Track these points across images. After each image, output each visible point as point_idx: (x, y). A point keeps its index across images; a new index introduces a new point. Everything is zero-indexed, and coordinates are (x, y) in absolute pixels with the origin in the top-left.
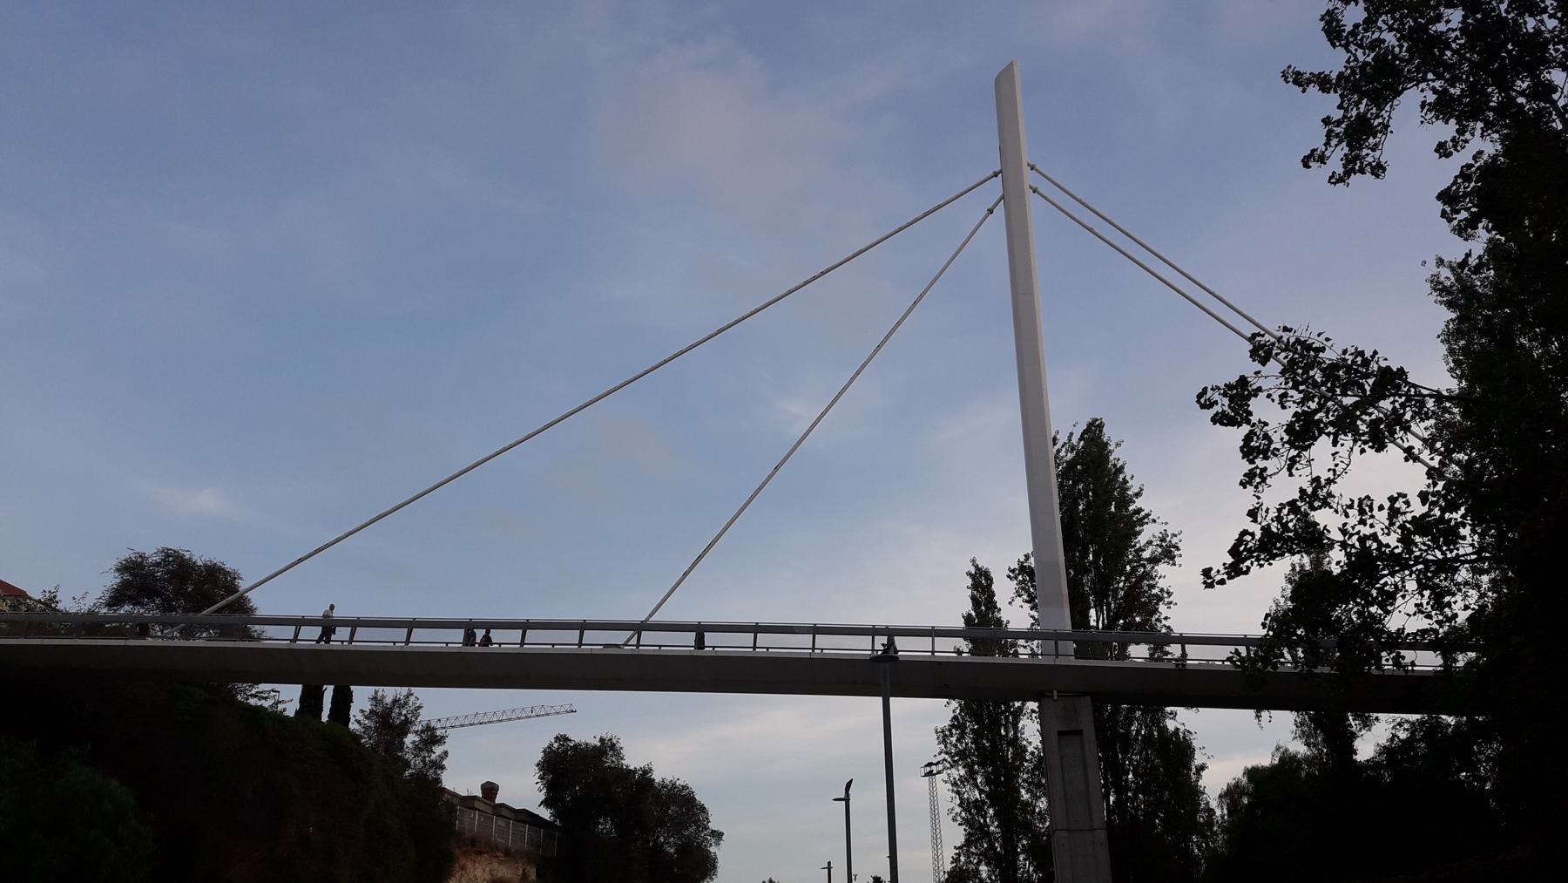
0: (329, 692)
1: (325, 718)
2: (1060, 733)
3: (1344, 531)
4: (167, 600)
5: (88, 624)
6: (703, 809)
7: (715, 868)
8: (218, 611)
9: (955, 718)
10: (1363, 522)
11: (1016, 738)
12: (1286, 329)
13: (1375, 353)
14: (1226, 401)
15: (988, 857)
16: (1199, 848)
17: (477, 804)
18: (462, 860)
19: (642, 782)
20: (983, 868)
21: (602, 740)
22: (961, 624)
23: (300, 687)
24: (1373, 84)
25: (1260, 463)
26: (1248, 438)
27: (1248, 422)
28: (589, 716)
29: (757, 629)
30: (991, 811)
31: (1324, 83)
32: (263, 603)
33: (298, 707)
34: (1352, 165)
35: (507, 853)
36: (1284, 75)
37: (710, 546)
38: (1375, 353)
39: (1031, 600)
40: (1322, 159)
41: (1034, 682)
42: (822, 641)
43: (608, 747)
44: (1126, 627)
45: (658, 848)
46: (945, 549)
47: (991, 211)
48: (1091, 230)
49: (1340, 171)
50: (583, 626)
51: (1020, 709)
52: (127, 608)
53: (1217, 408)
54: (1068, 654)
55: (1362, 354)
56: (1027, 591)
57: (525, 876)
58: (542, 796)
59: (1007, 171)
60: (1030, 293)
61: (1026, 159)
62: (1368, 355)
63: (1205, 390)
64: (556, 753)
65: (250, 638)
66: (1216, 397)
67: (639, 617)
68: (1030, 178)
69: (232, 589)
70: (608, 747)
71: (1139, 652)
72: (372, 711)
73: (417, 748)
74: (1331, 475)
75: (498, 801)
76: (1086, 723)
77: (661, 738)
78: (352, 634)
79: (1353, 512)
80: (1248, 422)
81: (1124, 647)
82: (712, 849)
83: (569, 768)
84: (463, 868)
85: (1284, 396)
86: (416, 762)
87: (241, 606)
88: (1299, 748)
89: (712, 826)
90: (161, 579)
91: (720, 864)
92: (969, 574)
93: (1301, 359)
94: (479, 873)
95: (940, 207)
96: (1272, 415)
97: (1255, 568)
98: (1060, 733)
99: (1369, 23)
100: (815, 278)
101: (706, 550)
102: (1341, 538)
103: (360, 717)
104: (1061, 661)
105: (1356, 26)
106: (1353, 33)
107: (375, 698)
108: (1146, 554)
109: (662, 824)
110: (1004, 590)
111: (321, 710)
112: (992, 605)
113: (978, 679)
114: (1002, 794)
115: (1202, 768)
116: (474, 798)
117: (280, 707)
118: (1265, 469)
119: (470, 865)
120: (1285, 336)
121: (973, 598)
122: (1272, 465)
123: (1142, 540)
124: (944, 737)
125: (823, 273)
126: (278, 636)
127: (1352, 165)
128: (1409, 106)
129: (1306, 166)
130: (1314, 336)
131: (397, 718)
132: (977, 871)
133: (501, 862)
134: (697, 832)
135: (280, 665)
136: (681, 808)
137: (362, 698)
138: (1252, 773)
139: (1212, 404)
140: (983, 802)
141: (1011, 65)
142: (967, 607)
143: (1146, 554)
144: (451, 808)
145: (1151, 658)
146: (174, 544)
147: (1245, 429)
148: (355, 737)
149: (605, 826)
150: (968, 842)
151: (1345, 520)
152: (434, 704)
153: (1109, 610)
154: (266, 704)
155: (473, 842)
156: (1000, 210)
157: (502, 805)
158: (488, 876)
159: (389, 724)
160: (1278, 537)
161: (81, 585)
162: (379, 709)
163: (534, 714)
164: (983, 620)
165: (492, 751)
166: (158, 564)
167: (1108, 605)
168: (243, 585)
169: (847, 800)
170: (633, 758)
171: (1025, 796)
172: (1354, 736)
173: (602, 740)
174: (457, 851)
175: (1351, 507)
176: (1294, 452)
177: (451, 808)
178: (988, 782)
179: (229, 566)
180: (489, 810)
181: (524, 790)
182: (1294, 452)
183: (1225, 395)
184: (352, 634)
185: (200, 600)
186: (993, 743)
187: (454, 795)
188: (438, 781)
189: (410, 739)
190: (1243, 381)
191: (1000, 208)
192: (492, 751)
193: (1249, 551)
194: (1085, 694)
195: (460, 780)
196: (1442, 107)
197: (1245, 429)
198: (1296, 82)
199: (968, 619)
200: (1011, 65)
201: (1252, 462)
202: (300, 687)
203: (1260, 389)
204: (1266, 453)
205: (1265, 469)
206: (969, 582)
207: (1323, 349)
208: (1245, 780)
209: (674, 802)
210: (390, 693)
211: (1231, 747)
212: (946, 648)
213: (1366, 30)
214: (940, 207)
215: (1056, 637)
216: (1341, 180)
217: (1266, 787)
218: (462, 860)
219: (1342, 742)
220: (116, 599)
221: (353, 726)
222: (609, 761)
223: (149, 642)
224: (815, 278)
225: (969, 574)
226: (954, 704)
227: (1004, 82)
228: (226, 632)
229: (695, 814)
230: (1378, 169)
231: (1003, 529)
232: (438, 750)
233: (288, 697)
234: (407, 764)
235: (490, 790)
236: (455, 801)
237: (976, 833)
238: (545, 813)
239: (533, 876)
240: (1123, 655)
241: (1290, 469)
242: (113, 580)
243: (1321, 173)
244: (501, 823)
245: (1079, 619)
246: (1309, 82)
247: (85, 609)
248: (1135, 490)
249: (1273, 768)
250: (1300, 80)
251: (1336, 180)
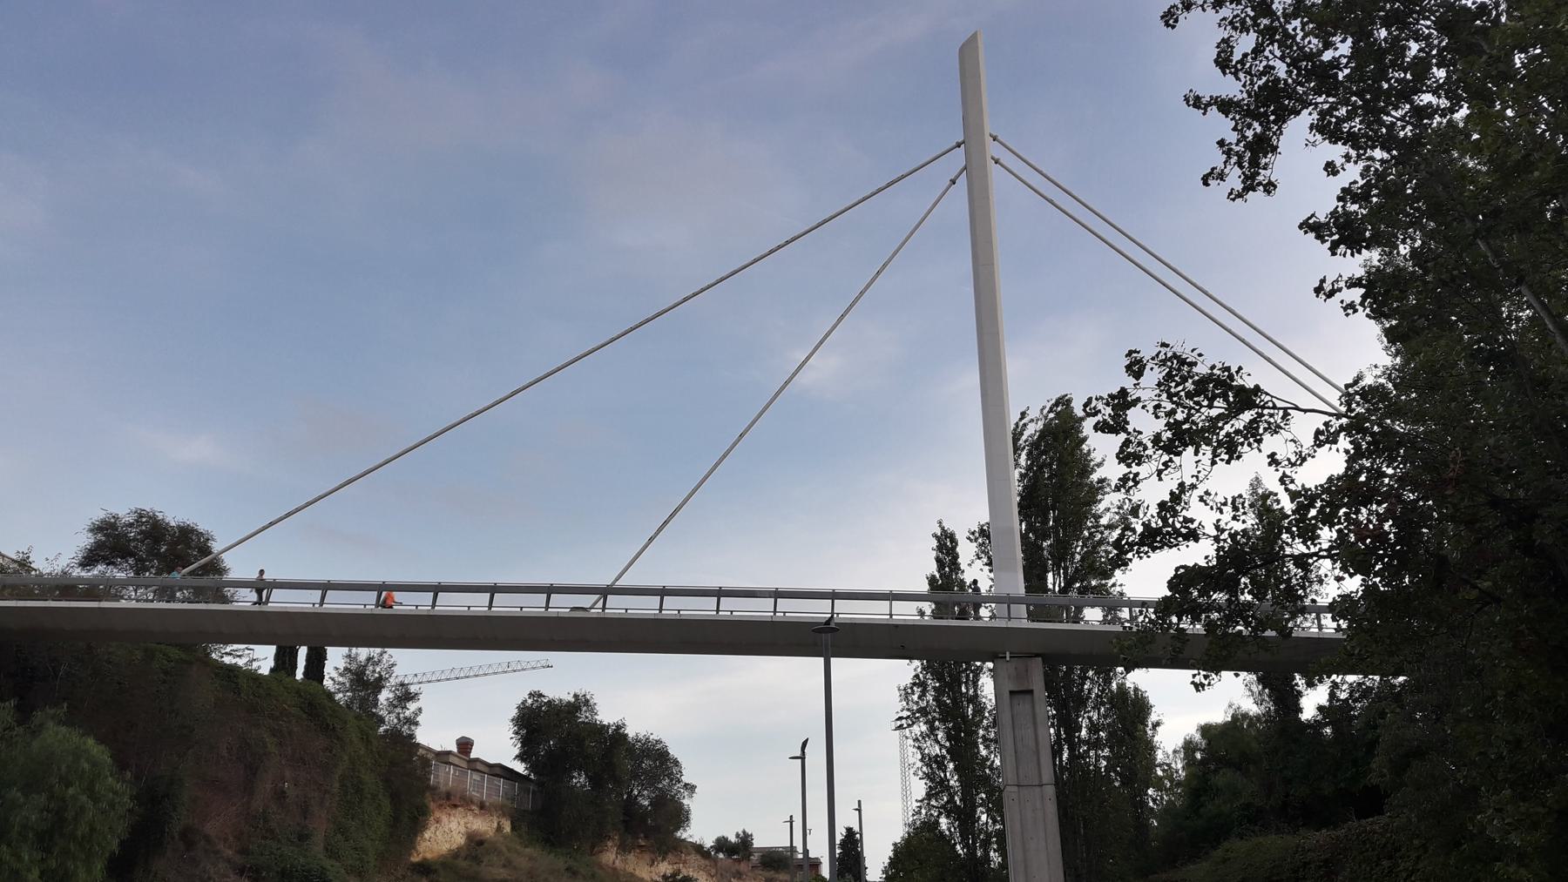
0: (303, 652)
1: (299, 675)
2: (1012, 693)
3: (1217, 527)
4: (140, 560)
5: (64, 587)
6: (676, 763)
7: (688, 819)
8: (191, 573)
9: (917, 676)
10: (1234, 518)
11: (976, 696)
12: (1164, 345)
13: (1240, 368)
14: (1109, 410)
15: (949, 810)
16: (1154, 800)
17: (452, 759)
18: (437, 814)
19: (616, 737)
20: (943, 821)
21: (576, 696)
22: (924, 587)
23: (274, 648)
24: (1266, 108)
25: (1135, 469)
26: (1127, 443)
27: (1125, 430)
28: (561, 675)
29: (720, 593)
30: (951, 766)
31: (1225, 106)
32: (239, 566)
33: (272, 664)
34: (1250, 184)
35: (482, 806)
36: (1187, 100)
37: (676, 512)
38: (1240, 368)
39: (989, 564)
40: (1221, 176)
41: (993, 645)
42: (783, 604)
43: (581, 703)
44: (1082, 591)
45: (632, 800)
46: (912, 515)
47: (953, 182)
48: (1051, 202)
49: (1239, 187)
50: (550, 590)
51: (981, 668)
52: (101, 567)
53: (1099, 417)
54: (1020, 619)
55: (1228, 369)
56: (987, 553)
57: (499, 828)
58: (517, 751)
59: (971, 141)
60: (990, 264)
61: (988, 129)
62: (1233, 370)
63: (1090, 400)
64: (530, 708)
65: (225, 600)
66: (1100, 406)
67: (605, 580)
68: (993, 149)
69: (205, 551)
70: (581, 703)
71: (1093, 615)
72: (346, 669)
73: (392, 706)
74: (1194, 480)
75: (473, 756)
76: (1038, 684)
77: (632, 696)
78: (323, 598)
79: (1228, 509)
80: (1125, 430)
81: (1079, 610)
82: (685, 802)
83: (546, 726)
84: (438, 821)
85: (1157, 407)
86: (391, 719)
87: (215, 568)
88: (1251, 707)
89: (685, 779)
90: (135, 539)
91: (692, 816)
92: (935, 535)
93: (1177, 367)
94: (454, 826)
95: (903, 177)
96: (1145, 423)
97: (1136, 560)
98: (1012, 693)
99: (1258, 51)
100: (780, 247)
101: (672, 516)
102: (1215, 533)
103: (334, 674)
104: (1013, 624)
105: (1245, 55)
106: (1242, 62)
107: (349, 656)
108: (1104, 521)
109: (636, 777)
110: (966, 551)
111: (295, 667)
112: (955, 566)
113: (942, 644)
114: (962, 748)
115: (1156, 725)
116: (449, 753)
117: (255, 665)
118: (1137, 474)
119: (445, 819)
120: (1164, 350)
121: (938, 560)
122: (1144, 470)
123: (1101, 507)
124: (906, 694)
125: (788, 242)
126: (245, 600)
127: (1250, 184)
128: (1299, 127)
129: (1206, 184)
130: (1188, 351)
131: (371, 674)
132: (937, 823)
133: (475, 815)
134: (671, 785)
135: (252, 628)
136: (655, 761)
137: (336, 658)
138: (1206, 730)
139: (1097, 412)
140: (944, 757)
141: (974, 37)
142: (932, 568)
143: (1104, 521)
144: (425, 762)
145: (1104, 622)
146: (147, 506)
147: (1123, 436)
148: (330, 695)
149: (580, 780)
150: (929, 796)
151: (1218, 515)
152: (406, 663)
153: (1065, 574)
154: (241, 662)
155: (448, 796)
156: (962, 181)
157: (477, 760)
158: (463, 829)
159: (364, 683)
160: (1158, 531)
161: (56, 549)
162: (354, 667)
163: (509, 669)
164: (946, 582)
165: (466, 709)
166: (131, 525)
167: (1066, 569)
168: (216, 547)
169: (803, 758)
170: (606, 715)
171: (984, 752)
172: (1300, 694)
173: (576, 696)
174: (432, 805)
175: (1225, 504)
176: (1166, 458)
177: (425, 762)
178: (949, 738)
179: (201, 528)
180: (464, 765)
181: (500, 746)
182: (1166, 458)
183: (1108, 404)
184: (323, 598)
185: (174, 561)
186: (954, 700)
187: (429, 750)
188: (412, 736)
189: (385, 696)
190: (1123, 392)
191: (963, 179)
192: (466, 709)
193: (1131, 545)
194: (1037, 655)
195: (434, 734)
196: (1328, 129)
197: (1123, 436)
198: (1195, 106)
199: (932, 580)
200: (974, 37)
201: (1129, 466)
202: (274, 648)
203: (1138, 400)
204: (1138, 459)
205: (1137, 474)
206: (935, 543)
207: (1195, 364)
208: (1197, 737)
209: (648, 757)
210: (363, 653)
211: (1185, 708)
212: (906, 612)
213: (1254, 59)
214: (903, 177)
215: (1009, 600)
216: (1240, 195)
217: (1220, 745)
218: (437, 814)
219: (1287, 701)
220: (89, 560)
221: (327, 683)
222: (583, 716)
223: (123, 604)
224: (780, 247)
225: (935, 535)
226: (917, 663)
227: (968, 52)
228: (199, 594)
229: (668, 768)
230: (1270, 187)
231: (961, 496)
232: (412, 706)
233: (262, 658)
234: (381, 720)
235: (465, 745)
236: (430, 756)
237: (937, 787)
238: (520, 767)
239: (507, 828)
240: (1077, 619)
241: (1160, 473)
242: (86, 540)
243: (1219, 189)
244: (476, 777)
245: (1034, 579)
246: (1209, 104)
247: (58, 570)
248: (1098, 460)
249: (1226, 724)
250: (1196, 102)
251: (1235, 196)
